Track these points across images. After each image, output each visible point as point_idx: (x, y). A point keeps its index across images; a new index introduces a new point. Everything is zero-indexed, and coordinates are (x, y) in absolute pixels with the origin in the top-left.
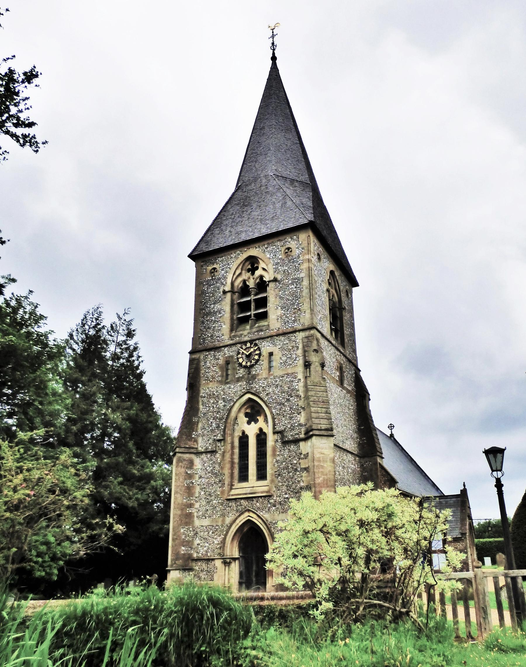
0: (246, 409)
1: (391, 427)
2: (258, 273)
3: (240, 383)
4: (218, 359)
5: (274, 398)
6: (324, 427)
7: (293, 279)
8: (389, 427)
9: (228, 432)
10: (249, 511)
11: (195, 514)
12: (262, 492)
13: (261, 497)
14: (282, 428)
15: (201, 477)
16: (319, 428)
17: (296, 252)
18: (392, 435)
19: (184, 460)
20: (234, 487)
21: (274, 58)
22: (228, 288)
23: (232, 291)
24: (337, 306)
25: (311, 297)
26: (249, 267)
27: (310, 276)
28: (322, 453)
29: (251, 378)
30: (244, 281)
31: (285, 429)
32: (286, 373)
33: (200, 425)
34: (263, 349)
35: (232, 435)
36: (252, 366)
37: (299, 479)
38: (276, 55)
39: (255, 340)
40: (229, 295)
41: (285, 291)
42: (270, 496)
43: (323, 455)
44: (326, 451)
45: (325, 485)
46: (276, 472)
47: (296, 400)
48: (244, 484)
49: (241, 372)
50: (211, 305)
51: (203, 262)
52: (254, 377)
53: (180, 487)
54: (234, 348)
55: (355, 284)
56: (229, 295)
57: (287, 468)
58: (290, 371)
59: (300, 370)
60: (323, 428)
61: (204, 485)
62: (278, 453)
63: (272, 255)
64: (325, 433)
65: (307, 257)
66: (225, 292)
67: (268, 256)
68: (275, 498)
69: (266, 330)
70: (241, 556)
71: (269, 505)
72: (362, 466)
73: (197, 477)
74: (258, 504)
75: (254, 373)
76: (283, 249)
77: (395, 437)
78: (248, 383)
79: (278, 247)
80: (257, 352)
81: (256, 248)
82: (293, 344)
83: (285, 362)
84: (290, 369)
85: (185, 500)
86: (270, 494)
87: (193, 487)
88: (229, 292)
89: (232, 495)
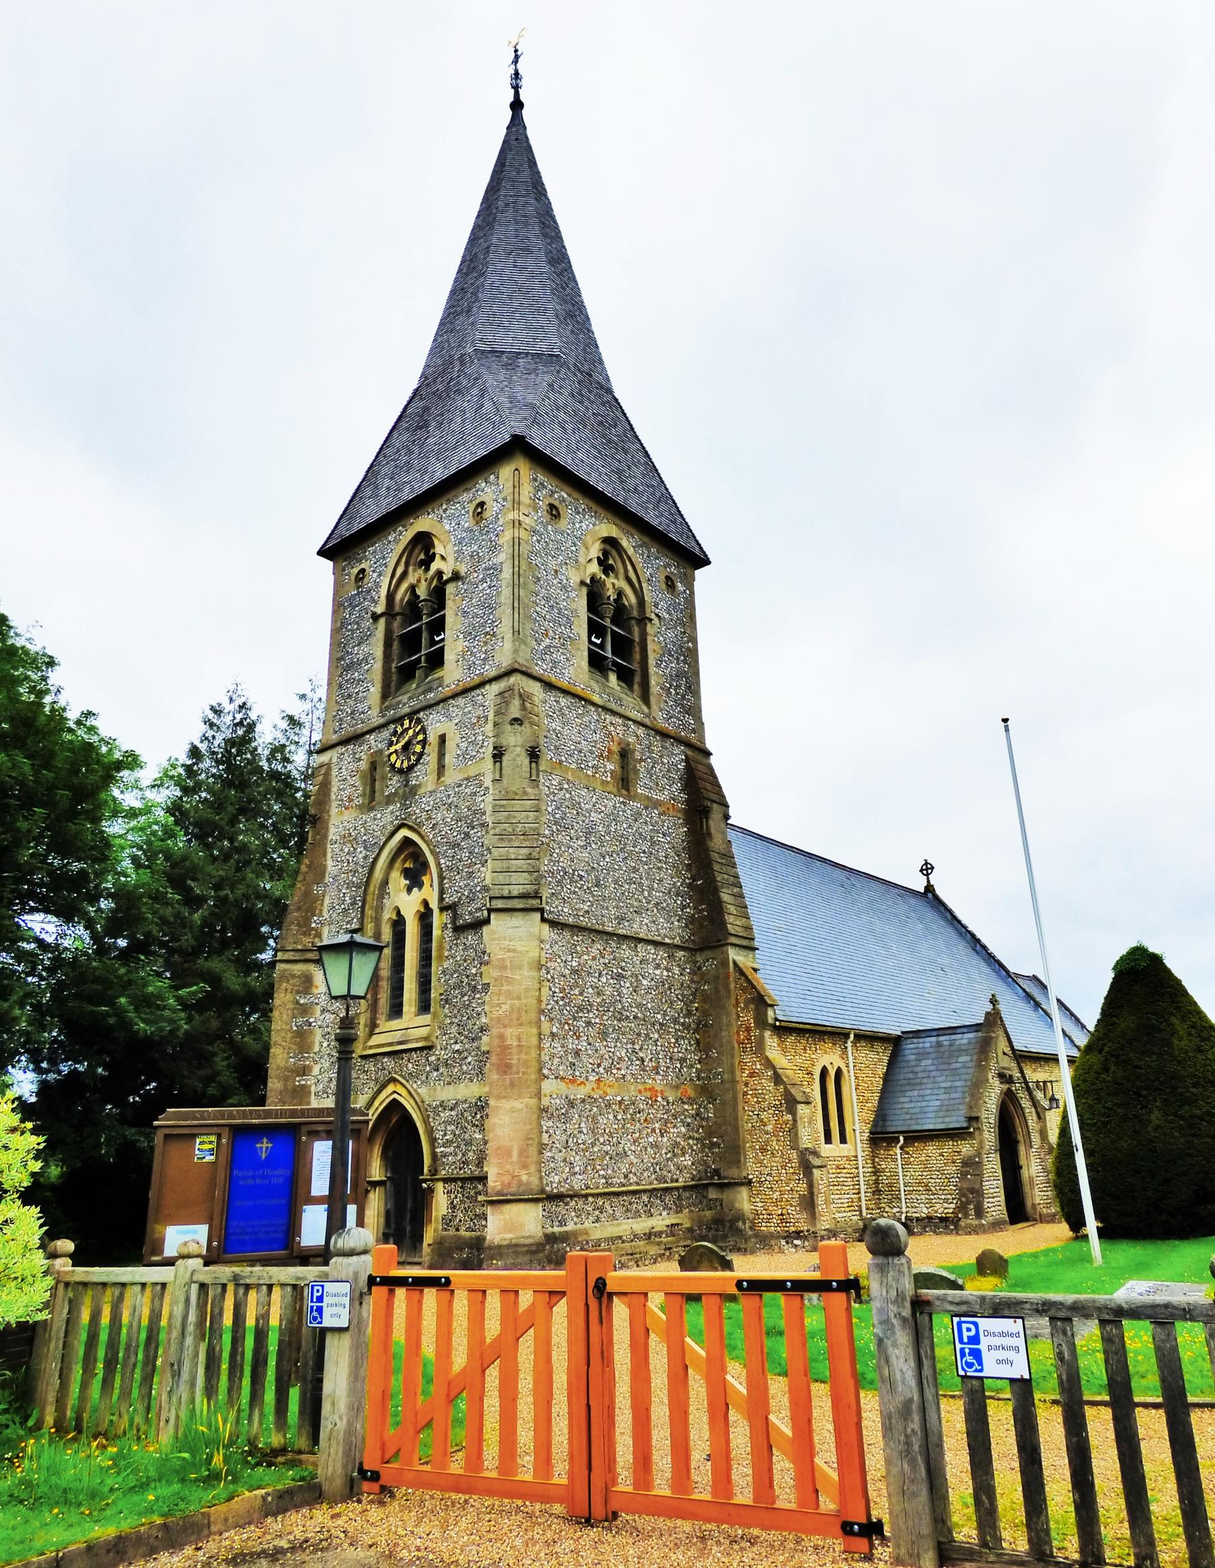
0: (404, 861)
1: (927, 869)
2: (434, 566)
3: (391, 807)
4: (360, 759)
5: (443, 833)
6: (516, 890)
7: (487, 569)
8: (921, 871)
9: (369, 912)
10: (394, 1080)
11: (313, 1089)
12: (417, 1040)
13: (415, 1050)
14: (455, 898)
15: (323, 1011)
16: (506, 893)
17: (492, 509)
18: (929, 888)
19: (293, 976)
20: (377, 1031)
21: (517, 105)
22: (380, 609)
23: (389, 613)
24: (635, 613)
25: (516, 605)
26: (422, 556)
27: (515, 557)
28: (509, 951)
29: (409, 793)
30: (412, 588)
31: (460, 899)
32: (466, 776)
33: (327, 901)
34: (430, 730)
35: (377, 920)
36: (411, 768)
37: (480, 1009)
38: (522, 98)
39: (418, 711)
40: (382, 621)
41: (471, 599)
42: (430, 1048)
43: (511, 954)
44: (519, 946)
45: (515, 1022)
46: (441, 994)
47: (479, 834)
48: (396, 1024)
49: (395, 782)
50: (353, 647)
51: (345, 560)
52: (413, 791)
53: (283, 1034)
54: (386, 734)
55: (697, 559)
56: (382, 621)
57: (459, 986)
58: (472, 772)
59: (487, 766)
60: (515, 893)
61: (327, 1027)
62: (446, 954)
63: (453, 524)
64: (518, 904)
65: (511, 516)
66: (375, 617)
67: (447, 527)
68: (437, 1053)
69: (437, 688)
70: (388, 1178)
71: (428, 1068)
72: (696, 970)
73: (318, 1009)
74: (410, 1065)
75: (414, 782)
76: (471, 507)
77: (938, 892)
78: (405, 807)
79: (462, 503)
80: (420, 737)
81: (429, 514)
82: (480, 712)
83: (466, 753)
84: (472, 767)
85: (292, 1060)
86: (430, 1044)
87: (311, 1032)
88: (382, 615)
89: (371, 1047)
